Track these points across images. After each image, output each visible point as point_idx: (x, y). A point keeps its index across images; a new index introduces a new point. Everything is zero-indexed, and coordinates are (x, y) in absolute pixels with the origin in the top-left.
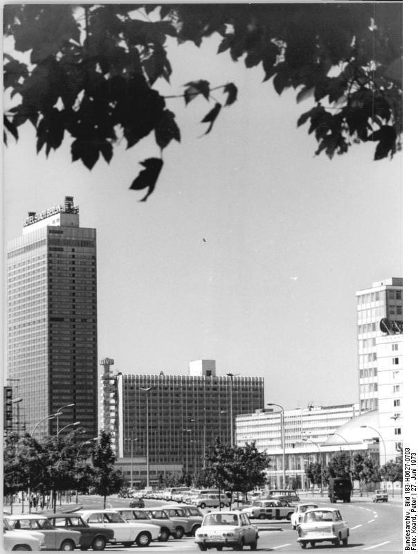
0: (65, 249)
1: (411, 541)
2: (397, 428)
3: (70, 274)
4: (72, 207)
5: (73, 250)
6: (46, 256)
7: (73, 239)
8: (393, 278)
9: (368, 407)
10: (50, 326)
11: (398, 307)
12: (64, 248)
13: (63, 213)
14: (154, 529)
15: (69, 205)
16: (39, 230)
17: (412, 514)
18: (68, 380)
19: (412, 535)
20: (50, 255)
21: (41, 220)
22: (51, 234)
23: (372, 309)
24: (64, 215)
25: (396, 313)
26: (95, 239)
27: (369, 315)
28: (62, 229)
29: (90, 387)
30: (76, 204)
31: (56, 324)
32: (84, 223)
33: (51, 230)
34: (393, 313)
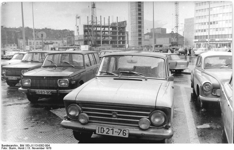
1: (6, 147)
14: (159, 50)
17: (17, 148)
19: (8, 148)
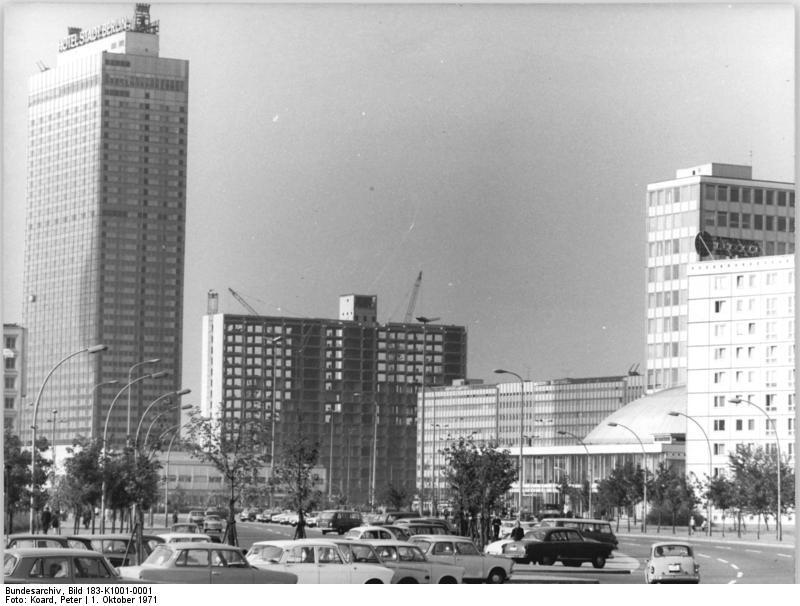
0: (131, 94)
2: (719, 419)
3: (141, 126)
4: (147, 22)
5: (147, 96)
6: (99, 103)
7: (148, 76)
8: (714, 164)
9: (660, 381)
10: (103, 224)
11: (719, 212)
12: (132, 91)
13: (131, 31)
15: (143, 19)
16: (87, 62)
17: (57, 598)
18: (132, 318)
20: (105, 103)
21: (90, 41)
22: (108, 67)
23: (666, 215)
24: (133, 34)
25: (716, 223)
26: (187, 77)
27: (669, 225)
28: (129, 59)
29: (169, 332)
30: (154, 16)
31: (112, 223)
32: (169, 47)
33: (109, 61)
34: (711, 223)
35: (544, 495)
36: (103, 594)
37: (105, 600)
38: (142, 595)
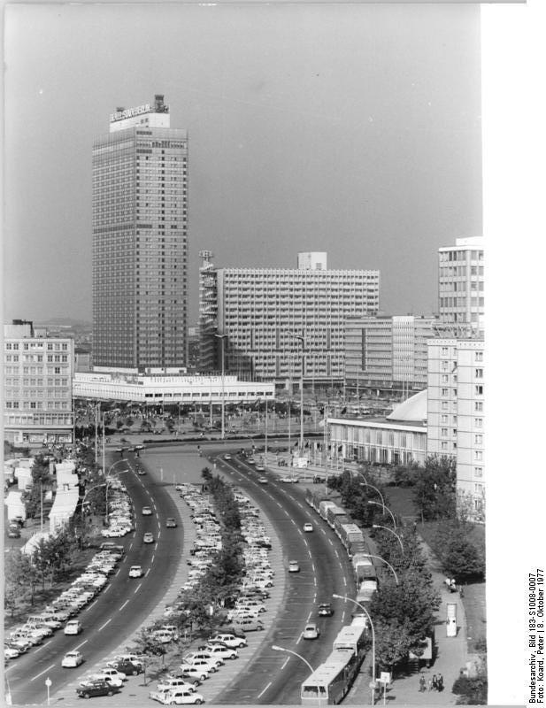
5: (163, 152)
12: (154, 150)
35: (366, 450)
36: (536, 617)
37: (540, 615)
38: (536, 582)
